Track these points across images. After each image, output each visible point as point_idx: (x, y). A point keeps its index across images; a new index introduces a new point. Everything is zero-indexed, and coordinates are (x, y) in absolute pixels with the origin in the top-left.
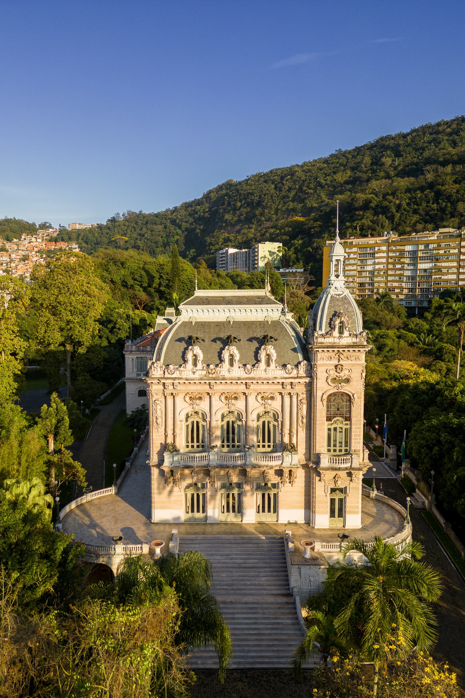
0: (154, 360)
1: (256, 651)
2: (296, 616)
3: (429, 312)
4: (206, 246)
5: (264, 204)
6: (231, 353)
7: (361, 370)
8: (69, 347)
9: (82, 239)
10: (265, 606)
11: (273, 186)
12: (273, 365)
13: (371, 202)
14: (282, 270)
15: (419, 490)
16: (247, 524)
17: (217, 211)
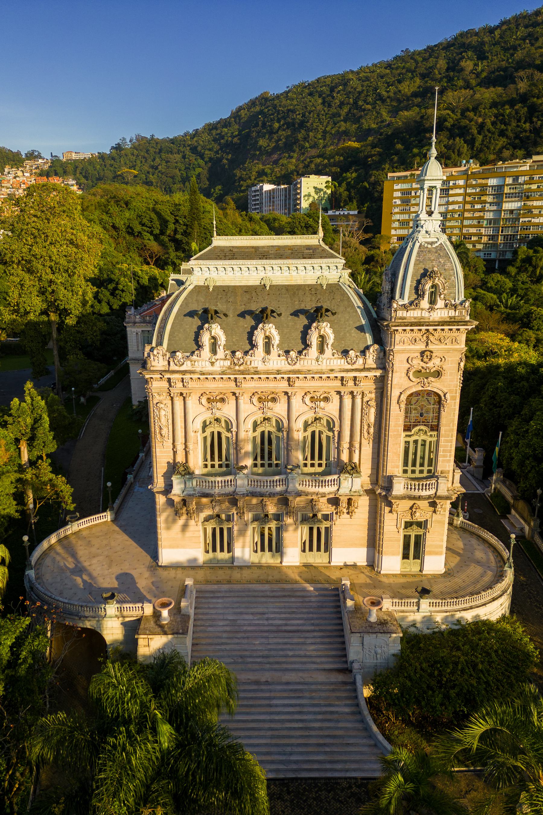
0: (154, 344)
1: (301, 753)
2: (343, 646)
3: (513, 266)
4: (235, 181)
5: (308, 124)
6: (267, 334)
7: (458, 359)
8: (53, 317)
9: (81, 173)
10: (313, 687)
11: (320, 101)
12: (328, 351)
13: (446, 121)
14: (330, 213)
15: (516, 511)
16: (289, 567)
17: (248, 135)
